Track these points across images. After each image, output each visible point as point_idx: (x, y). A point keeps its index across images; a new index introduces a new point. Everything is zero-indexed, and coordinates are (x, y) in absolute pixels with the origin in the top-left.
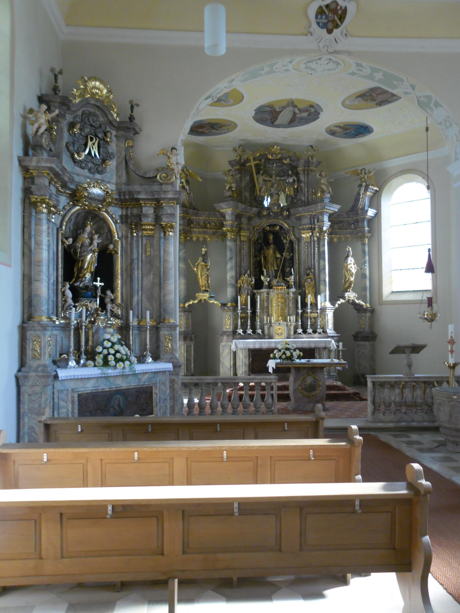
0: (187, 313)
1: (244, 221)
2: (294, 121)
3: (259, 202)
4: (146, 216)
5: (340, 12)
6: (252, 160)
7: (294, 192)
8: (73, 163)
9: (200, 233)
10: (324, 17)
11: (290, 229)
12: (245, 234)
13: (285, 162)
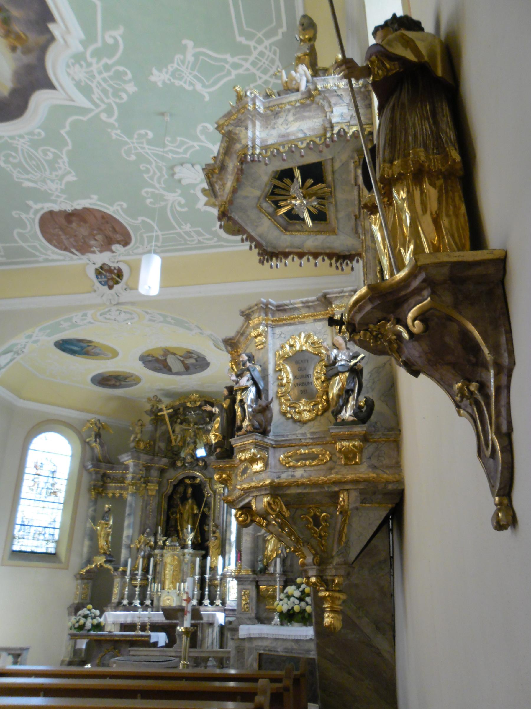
0: (86, 581)
1: (154, 473)
2: (188, 369)
3: (175, 453)
5: (116, 271)
6: (164, 409)
9: (116, 488)
10: (103, 277)
11: (206, 481)
12: (152, 487)
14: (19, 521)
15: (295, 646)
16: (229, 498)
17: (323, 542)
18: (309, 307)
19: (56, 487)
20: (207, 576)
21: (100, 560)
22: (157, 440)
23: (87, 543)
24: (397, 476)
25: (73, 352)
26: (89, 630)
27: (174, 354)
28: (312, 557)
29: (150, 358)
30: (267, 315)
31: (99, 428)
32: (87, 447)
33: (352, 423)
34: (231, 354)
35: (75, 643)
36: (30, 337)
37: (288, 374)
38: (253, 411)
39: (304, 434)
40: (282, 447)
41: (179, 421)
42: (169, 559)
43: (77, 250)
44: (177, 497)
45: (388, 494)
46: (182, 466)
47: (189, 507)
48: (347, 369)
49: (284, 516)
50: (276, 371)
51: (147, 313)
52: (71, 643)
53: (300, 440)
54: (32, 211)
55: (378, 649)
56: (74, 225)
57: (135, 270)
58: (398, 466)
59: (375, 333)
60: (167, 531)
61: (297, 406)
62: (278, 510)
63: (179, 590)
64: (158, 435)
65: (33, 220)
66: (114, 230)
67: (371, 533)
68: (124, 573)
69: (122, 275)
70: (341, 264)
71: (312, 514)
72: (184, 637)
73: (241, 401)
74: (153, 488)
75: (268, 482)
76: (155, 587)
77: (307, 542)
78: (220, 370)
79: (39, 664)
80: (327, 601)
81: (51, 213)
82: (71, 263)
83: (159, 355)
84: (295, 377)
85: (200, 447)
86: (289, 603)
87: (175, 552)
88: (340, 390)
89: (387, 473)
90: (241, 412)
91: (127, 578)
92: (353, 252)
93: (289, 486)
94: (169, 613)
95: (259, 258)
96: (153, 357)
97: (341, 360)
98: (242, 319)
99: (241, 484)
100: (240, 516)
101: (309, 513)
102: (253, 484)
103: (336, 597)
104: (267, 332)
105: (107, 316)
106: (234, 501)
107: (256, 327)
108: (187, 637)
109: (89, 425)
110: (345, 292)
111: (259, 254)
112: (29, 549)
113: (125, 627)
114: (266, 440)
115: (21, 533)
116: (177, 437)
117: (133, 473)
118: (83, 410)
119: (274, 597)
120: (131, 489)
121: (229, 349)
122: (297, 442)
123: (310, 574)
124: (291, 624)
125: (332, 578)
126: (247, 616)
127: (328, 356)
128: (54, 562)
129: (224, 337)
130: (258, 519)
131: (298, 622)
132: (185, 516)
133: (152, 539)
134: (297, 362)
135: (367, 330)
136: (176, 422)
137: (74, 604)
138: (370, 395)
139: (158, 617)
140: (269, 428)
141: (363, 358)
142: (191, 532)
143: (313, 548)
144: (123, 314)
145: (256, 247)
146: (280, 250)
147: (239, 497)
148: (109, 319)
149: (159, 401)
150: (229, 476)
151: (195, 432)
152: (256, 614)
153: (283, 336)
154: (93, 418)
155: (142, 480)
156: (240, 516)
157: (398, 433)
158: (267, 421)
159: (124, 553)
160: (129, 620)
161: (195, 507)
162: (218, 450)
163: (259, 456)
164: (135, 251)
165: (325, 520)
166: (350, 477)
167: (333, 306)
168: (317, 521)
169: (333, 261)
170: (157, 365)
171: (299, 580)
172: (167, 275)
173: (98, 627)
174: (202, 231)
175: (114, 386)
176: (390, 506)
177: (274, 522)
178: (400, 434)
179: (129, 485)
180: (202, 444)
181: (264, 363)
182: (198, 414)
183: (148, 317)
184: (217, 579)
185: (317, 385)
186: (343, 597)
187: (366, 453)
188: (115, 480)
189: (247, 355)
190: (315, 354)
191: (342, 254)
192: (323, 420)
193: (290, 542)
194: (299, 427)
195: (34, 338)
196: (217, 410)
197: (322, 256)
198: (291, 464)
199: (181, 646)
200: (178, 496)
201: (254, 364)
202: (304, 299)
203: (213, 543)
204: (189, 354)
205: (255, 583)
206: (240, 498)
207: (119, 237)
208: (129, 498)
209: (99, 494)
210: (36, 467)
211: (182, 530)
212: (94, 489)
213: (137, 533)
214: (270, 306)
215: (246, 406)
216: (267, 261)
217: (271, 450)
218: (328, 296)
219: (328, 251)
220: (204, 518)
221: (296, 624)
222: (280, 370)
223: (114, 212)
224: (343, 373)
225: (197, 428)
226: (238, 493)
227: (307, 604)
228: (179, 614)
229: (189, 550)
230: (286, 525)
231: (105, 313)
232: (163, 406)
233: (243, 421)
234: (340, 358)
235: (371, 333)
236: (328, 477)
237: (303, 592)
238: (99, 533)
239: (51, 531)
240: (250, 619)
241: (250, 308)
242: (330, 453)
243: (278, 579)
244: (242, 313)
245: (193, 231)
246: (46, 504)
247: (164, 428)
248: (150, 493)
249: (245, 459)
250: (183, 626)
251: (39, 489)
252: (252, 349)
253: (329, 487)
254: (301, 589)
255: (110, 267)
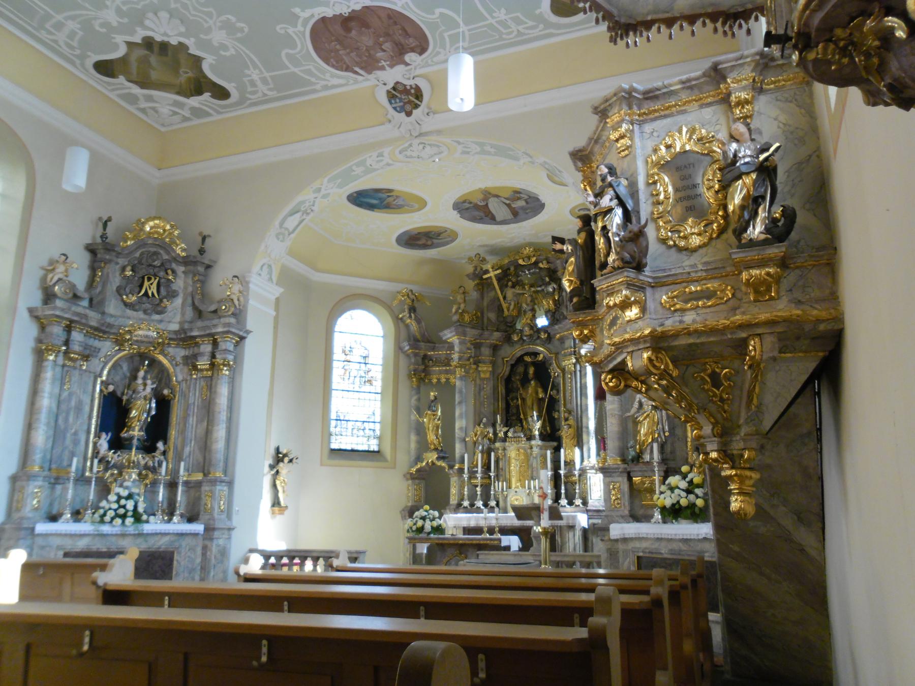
0: (417, 481)
1: (486, 351)
2: (516, 215)
4: (202, 354)
5: (413, 91)
7: (555, 305)
8: (123, 307)
9: (440, 372)
13: (541, 265)
14: (333, 416)
15: (683, 547)
16: (595, 359)
17: (726, 407)
18: (691, 88)
19: (370, 374)
20: (562, 472)
21: (432, 457)
22: (485, 311)
23: (413, 438)
24: (832, 311)
25: (371, 207)
26: (429, 533)
27: (497, 196)
28: (711, 427)
29: (467, 205)
30: (630, 108)
31: (413, 301)
32: (401, 325)
33: (765, 243)
34: (584, 171)
35: (414, 548)
36: (319, 190)
37: (667, 186)
38: (620, 240)
39: (694, 266)
40: (664, 285)
41: (510, 284)
42: (514, 453)
43: (362, 68)
44: (516, 379)
45: (817, 339)
46: (519, 340)
47: (532, 390)
48: (753, 169)
49: (671, 375)
50: (648, 184)
51: (459, 143)
52: (409, 547)
53: (689, 273)
54: (300, 21)
55: (801, 545)
56: (354, 33)
57: (440, 84)
58: (833, 298)
59: (842, 44)
60: (507, 420)
61: (682, 229)
62: (662, 367)
63: (529, 488)
64: (485, 304)
65: (303, 34)
66: (406, 34)
67: (793, 392)
68: (461, 470)
69: (422, 95)
70: (731, 27)
71: (709, 371)
72: (543, 539)
73: (604, 228)
74: (485, 369)
75: (647, 332)
76: (498, 486)
77: (703, 409)
78: (562, 205)
79: (379, 563)
80: (733, 482)
81: (324, 20)
82: (356, 87)
83: (477, 199)
84: (676, 190)
85: (540, 316)
86: (673, 495)
87: (520, 445)
88: (743, 199)
89: (816, 309)
90: (604, 243)
91: (466, 476)
92: (749, 6)
93: (676, 335)
94: (521, 512)
95: (609, 34)
96: (470, 203)
97: (744, 157)
98: (596, 117)
99: (609, 338)
100: (611, 381)
101: (705, 370)
102: (627, 336)
103: (747, 477)
104: (632, 131)
105: (409, 153)
106: (601, 362)
107: (616, 127)
108: (546, 538)
109: (400, 297)
110: (747, 57)
111: (609, 29)
112: (349, 448)
113: (467, 530)
114: (641, 278)
115: (338, 429)
116: (510, 304)
117: (459, 353)
118: (390, 280)
119: (652, 491)
120: (459, 372)
121: (580, 164)
122: (685, 277)
123: (709, 447)
124: (677, 520)
125: (740, 452)
126: (619, 513)
127: (725, 153)
128: (377, 461)
129: (571, 149)
130: (635, 383)
131: (686, 518)
132: (529, 402)
133: (491, 430)
134: (678, 169)
135: (830, 40)
136: (507, 286)
137: (406, 507)
138: (789, 202)
139: (510, 519)
140: (644, 261)
141: (778, 148)
142: (538, 420)
143: (711, 415)
144: (428, 148)
145: (604, 18)
146: (639, 19)
147: (609, 356)
148: (411, 157)
149: (484, 260)
150: (591, 331)
151: (531, 296)
152: (630, 511)
153: (655, 134)
154: (404, 288)
155: (471, 360)
156: (611, 381)
157: (833, 252)
158: (641, 252)
159: (458, 448)
160: (473, 524)
161: (540, 390)
162: (575, 300)
163: (633, 299)
164: (435, 59)
165: (728, 378)
166: (763, 317)
167: (729, 80)
168: (716, 380)
169: (719, 25)
170: (476, 213)
171: (685, 469)
172: (484, 82)
173: (439, 530)
174: (521, 17)
175: (425, 247)
176: (821, 354)
177: (656, 386)
178: (835, 254)
179: (456, 367)
180: (543, 311)
181: (632, 175)
182: (534, 273)
183: (460, 148)
184: (575, 475)
185: (709, 197)
186: (755, 476)
187: (785, 284)
188: (438, 362)
189: (606, 166)
190: (704, 154)
191: (732, 11)
192: (719, 244)
193: (681, 410)
194: (686, 258)
195: (323, 192)
196: (570, 248)
197: (701, 19)
198: (678, 306)
199: (540, 551)
200: (518, 377)
201: (617, 177)
202: (684, 77)
203: (566, 433)
204: (517, 194)
205: (626, 475)
206: (610, 357)
207: (412, 42)
208: (458, 383)
209: (421, 380)
210: (344, 352)
211: (526, 419)
212: (414, 374)
213: (471, 426)
214: (634, 94)
215: (610, 234)
216: (622, 38)
217: (649, 291)
218: (720, 67)
219: (710, 10)
220: (553, 403)
221: (684, 521)
222: (655, 183)
223: (403, 7)
224: (748, 174)
225: (534, 292)
226: (606, 350)
227: (697, 497)
228: (534, 513)
229: (537, 442)
230: (674, 388)
231: (405, 150)
232: (488, 267)
233: (608, 254)
234: (743, 153)
235: (836, 43)
236: (732, 319)
237: (691, 482)
238: (426, 425)
239: (372, 426)
240: (622, 517)
241: (607, 101)
242: (732, 287)
243: (656, 469)
244: (596, 110)
245: (510, 18)
246: (362, 395)
247: (492, 294)
248: (482, 375)
249: (615, 305)
250: (540, 525)
251: (352, 378)
252: (612, 159)
253: (731, 334)
254: (687, 479)
255: (405, 86)
